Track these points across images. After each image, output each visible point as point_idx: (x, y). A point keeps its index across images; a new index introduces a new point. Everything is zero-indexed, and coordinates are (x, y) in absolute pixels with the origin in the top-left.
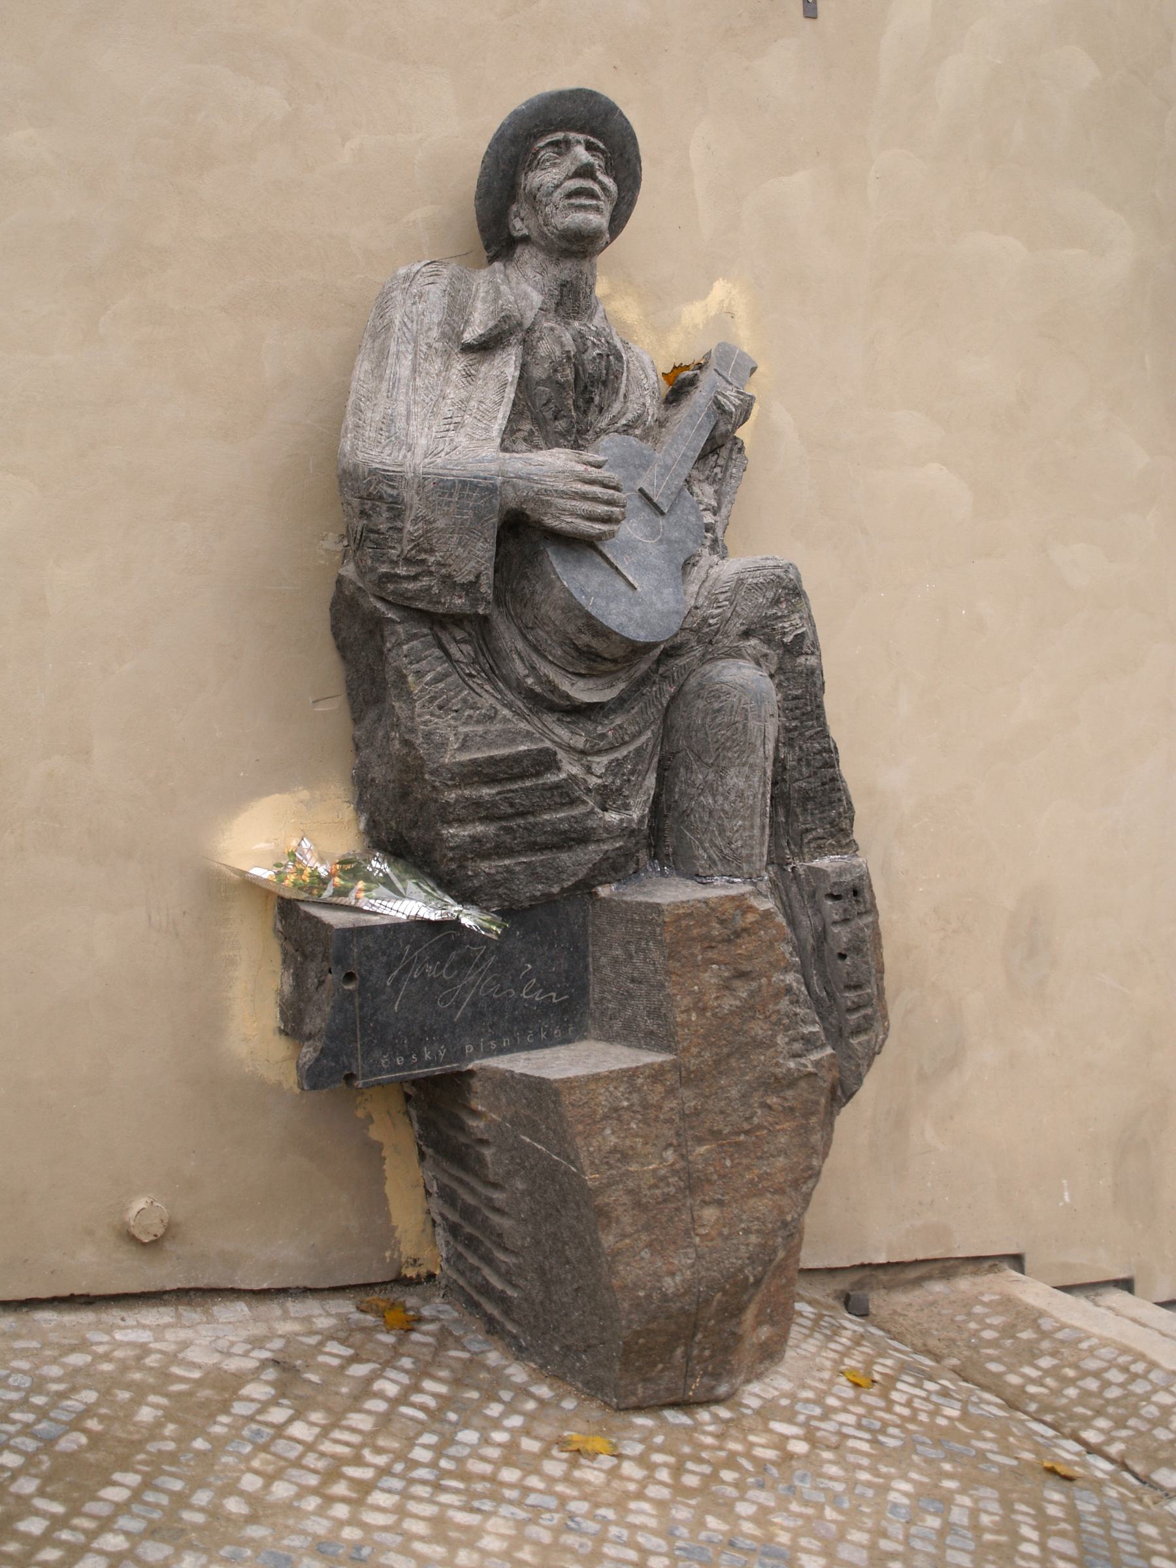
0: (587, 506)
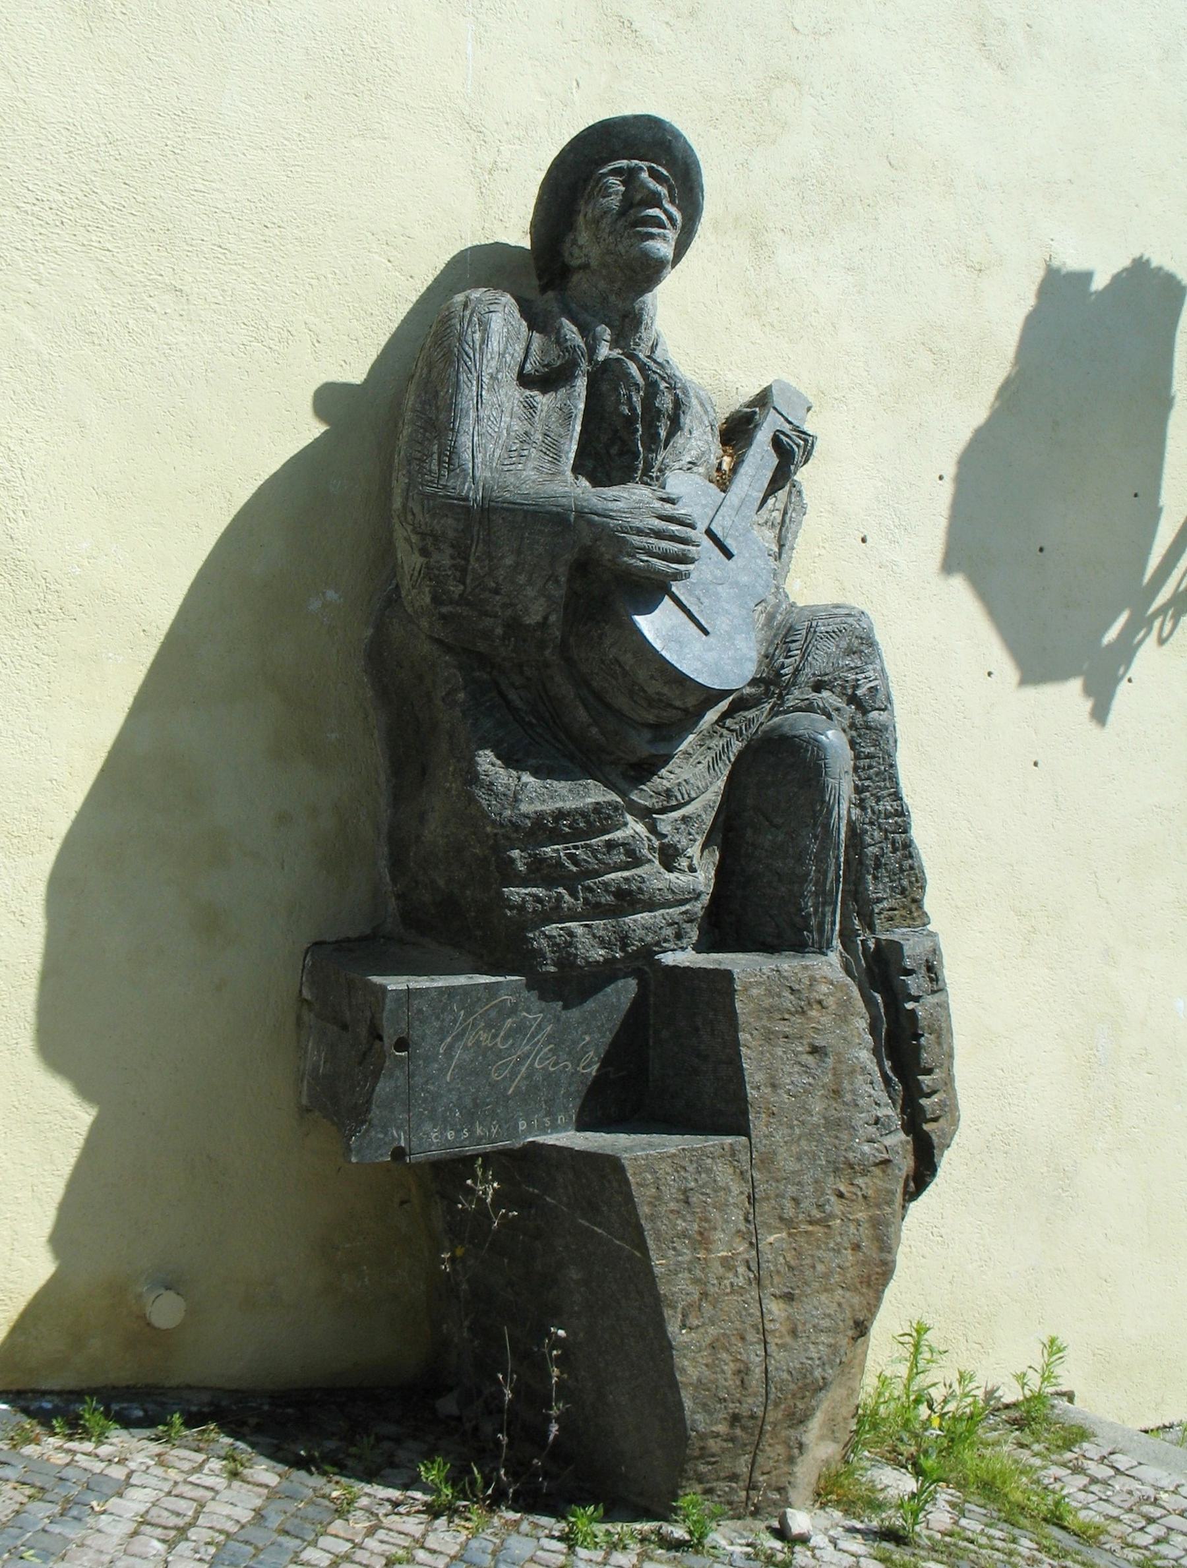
0: (665, 545)
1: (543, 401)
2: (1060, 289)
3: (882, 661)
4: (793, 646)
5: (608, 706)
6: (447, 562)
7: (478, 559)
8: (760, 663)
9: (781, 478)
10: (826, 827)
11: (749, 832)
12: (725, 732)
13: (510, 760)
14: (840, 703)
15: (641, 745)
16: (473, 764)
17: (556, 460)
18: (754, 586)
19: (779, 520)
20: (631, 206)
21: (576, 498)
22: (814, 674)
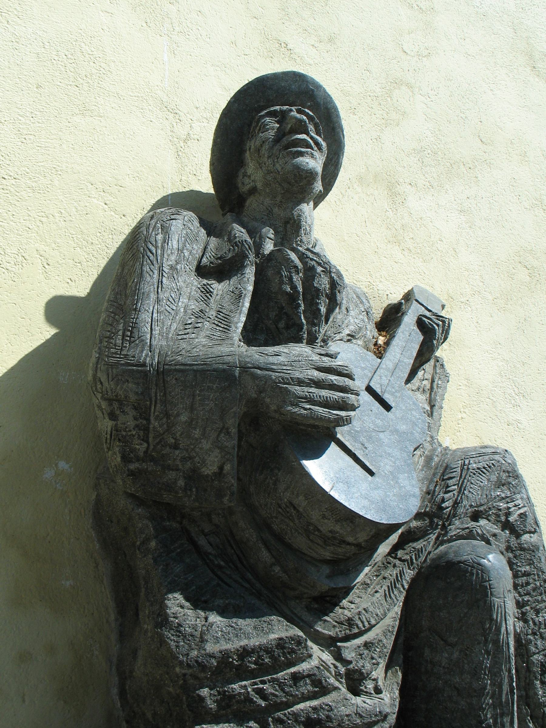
0: (325, 393)
1: (219, 288)
2: (366, 641)
3: (526, 490)
4: (451, 482)
5: (289, 546)
6: (131, 423)
7: (157, 418)
8: (423, 499)
9: (425, 353)
10: (496, 642)
11: (427, 652)
12: (397, 562)
13: (199, 602)
14: (496, 529)
15: (321, 580)
16: (163, 607)
17: (227, 329)
18: (412, 433)
19: (428, 386)
20: (284, 135)
21: (240, 356)
22: (471, 506)
